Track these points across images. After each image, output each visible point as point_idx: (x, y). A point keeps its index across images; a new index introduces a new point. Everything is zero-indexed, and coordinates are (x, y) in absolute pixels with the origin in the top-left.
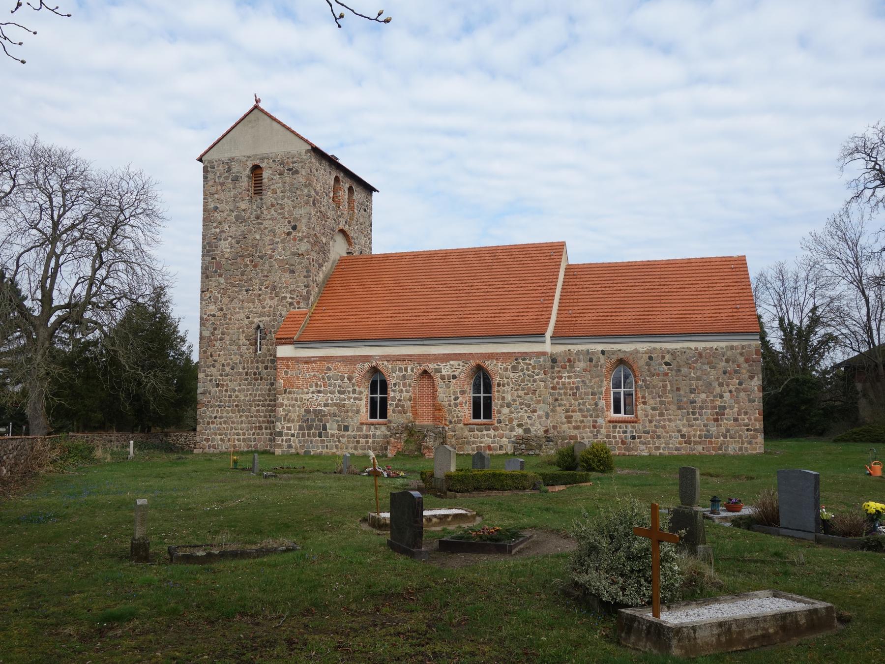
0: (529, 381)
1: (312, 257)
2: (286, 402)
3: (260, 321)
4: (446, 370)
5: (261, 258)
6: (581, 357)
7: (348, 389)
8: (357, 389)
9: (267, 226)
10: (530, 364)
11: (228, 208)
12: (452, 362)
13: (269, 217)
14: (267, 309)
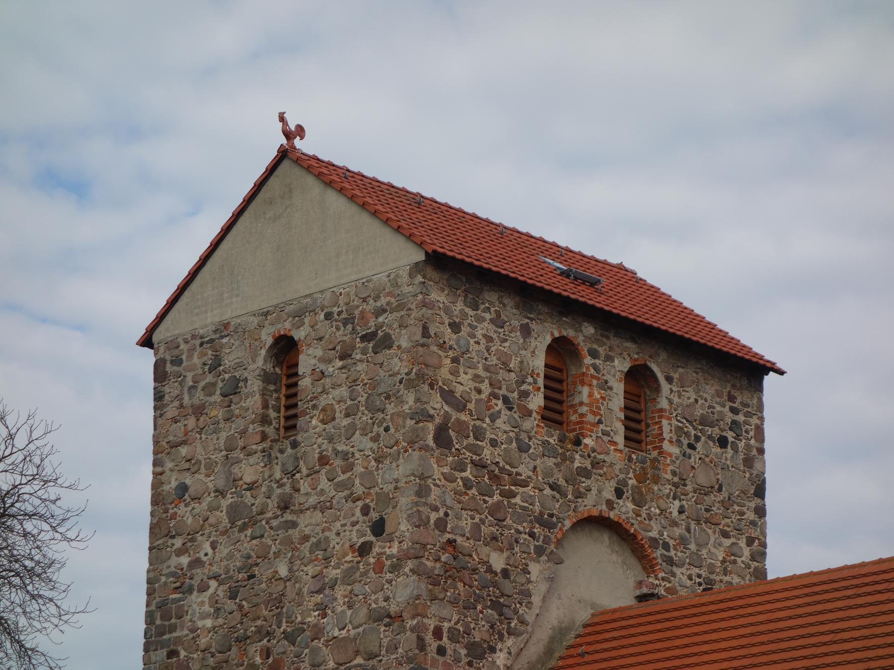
1: (431, 623)
5: (290, 638)
11: (211, 485)
13: (313, 500)
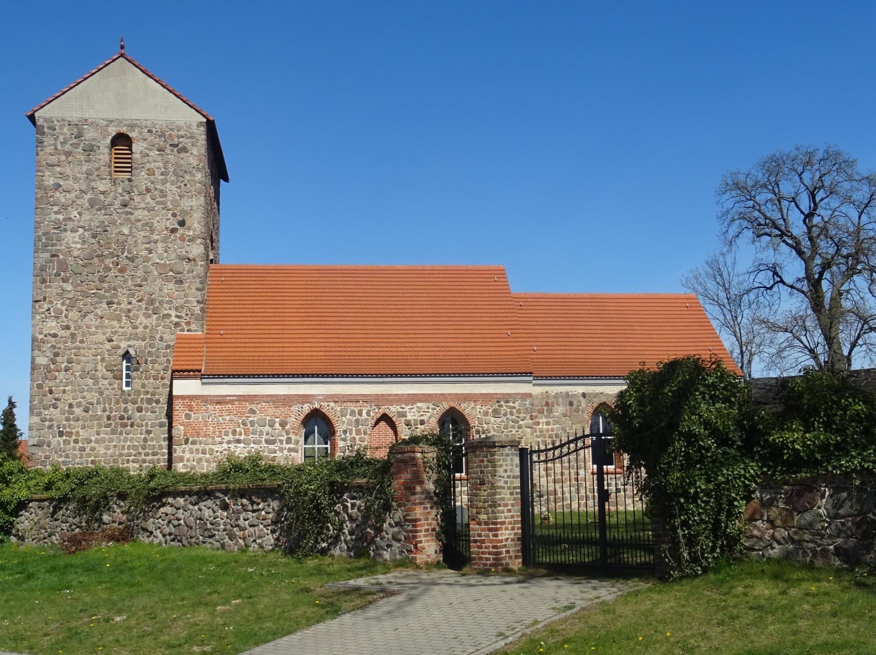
0: (513, 427)
2: (187, 455)
3: (130, 346)
4: (412, 414)
5: (132, 260)
6: (560, 400)
7: (280, 438)
8: (293, 437)
9: (139, 218)
10: (514, 408)
12: (419, 404)
13: (142, 205)
14: (140, 330)
